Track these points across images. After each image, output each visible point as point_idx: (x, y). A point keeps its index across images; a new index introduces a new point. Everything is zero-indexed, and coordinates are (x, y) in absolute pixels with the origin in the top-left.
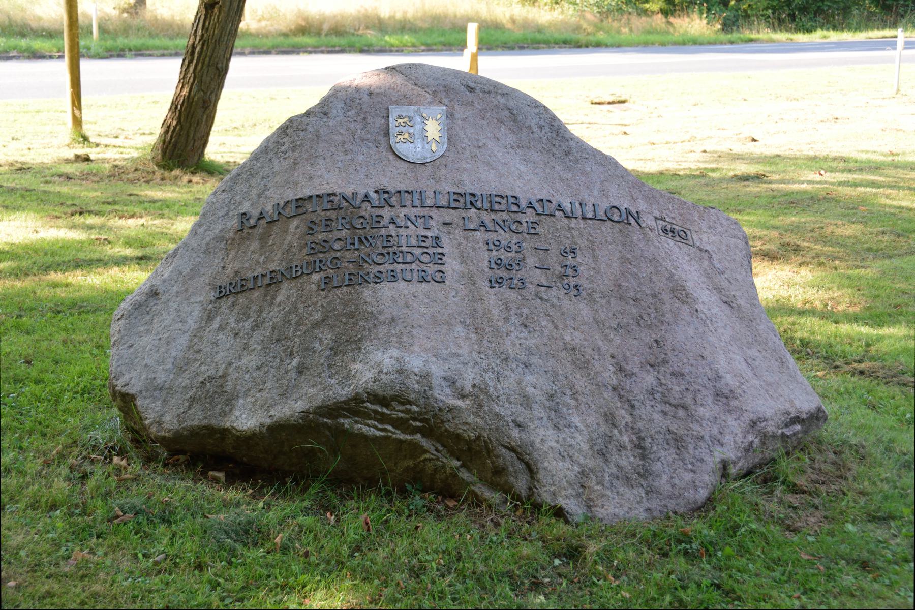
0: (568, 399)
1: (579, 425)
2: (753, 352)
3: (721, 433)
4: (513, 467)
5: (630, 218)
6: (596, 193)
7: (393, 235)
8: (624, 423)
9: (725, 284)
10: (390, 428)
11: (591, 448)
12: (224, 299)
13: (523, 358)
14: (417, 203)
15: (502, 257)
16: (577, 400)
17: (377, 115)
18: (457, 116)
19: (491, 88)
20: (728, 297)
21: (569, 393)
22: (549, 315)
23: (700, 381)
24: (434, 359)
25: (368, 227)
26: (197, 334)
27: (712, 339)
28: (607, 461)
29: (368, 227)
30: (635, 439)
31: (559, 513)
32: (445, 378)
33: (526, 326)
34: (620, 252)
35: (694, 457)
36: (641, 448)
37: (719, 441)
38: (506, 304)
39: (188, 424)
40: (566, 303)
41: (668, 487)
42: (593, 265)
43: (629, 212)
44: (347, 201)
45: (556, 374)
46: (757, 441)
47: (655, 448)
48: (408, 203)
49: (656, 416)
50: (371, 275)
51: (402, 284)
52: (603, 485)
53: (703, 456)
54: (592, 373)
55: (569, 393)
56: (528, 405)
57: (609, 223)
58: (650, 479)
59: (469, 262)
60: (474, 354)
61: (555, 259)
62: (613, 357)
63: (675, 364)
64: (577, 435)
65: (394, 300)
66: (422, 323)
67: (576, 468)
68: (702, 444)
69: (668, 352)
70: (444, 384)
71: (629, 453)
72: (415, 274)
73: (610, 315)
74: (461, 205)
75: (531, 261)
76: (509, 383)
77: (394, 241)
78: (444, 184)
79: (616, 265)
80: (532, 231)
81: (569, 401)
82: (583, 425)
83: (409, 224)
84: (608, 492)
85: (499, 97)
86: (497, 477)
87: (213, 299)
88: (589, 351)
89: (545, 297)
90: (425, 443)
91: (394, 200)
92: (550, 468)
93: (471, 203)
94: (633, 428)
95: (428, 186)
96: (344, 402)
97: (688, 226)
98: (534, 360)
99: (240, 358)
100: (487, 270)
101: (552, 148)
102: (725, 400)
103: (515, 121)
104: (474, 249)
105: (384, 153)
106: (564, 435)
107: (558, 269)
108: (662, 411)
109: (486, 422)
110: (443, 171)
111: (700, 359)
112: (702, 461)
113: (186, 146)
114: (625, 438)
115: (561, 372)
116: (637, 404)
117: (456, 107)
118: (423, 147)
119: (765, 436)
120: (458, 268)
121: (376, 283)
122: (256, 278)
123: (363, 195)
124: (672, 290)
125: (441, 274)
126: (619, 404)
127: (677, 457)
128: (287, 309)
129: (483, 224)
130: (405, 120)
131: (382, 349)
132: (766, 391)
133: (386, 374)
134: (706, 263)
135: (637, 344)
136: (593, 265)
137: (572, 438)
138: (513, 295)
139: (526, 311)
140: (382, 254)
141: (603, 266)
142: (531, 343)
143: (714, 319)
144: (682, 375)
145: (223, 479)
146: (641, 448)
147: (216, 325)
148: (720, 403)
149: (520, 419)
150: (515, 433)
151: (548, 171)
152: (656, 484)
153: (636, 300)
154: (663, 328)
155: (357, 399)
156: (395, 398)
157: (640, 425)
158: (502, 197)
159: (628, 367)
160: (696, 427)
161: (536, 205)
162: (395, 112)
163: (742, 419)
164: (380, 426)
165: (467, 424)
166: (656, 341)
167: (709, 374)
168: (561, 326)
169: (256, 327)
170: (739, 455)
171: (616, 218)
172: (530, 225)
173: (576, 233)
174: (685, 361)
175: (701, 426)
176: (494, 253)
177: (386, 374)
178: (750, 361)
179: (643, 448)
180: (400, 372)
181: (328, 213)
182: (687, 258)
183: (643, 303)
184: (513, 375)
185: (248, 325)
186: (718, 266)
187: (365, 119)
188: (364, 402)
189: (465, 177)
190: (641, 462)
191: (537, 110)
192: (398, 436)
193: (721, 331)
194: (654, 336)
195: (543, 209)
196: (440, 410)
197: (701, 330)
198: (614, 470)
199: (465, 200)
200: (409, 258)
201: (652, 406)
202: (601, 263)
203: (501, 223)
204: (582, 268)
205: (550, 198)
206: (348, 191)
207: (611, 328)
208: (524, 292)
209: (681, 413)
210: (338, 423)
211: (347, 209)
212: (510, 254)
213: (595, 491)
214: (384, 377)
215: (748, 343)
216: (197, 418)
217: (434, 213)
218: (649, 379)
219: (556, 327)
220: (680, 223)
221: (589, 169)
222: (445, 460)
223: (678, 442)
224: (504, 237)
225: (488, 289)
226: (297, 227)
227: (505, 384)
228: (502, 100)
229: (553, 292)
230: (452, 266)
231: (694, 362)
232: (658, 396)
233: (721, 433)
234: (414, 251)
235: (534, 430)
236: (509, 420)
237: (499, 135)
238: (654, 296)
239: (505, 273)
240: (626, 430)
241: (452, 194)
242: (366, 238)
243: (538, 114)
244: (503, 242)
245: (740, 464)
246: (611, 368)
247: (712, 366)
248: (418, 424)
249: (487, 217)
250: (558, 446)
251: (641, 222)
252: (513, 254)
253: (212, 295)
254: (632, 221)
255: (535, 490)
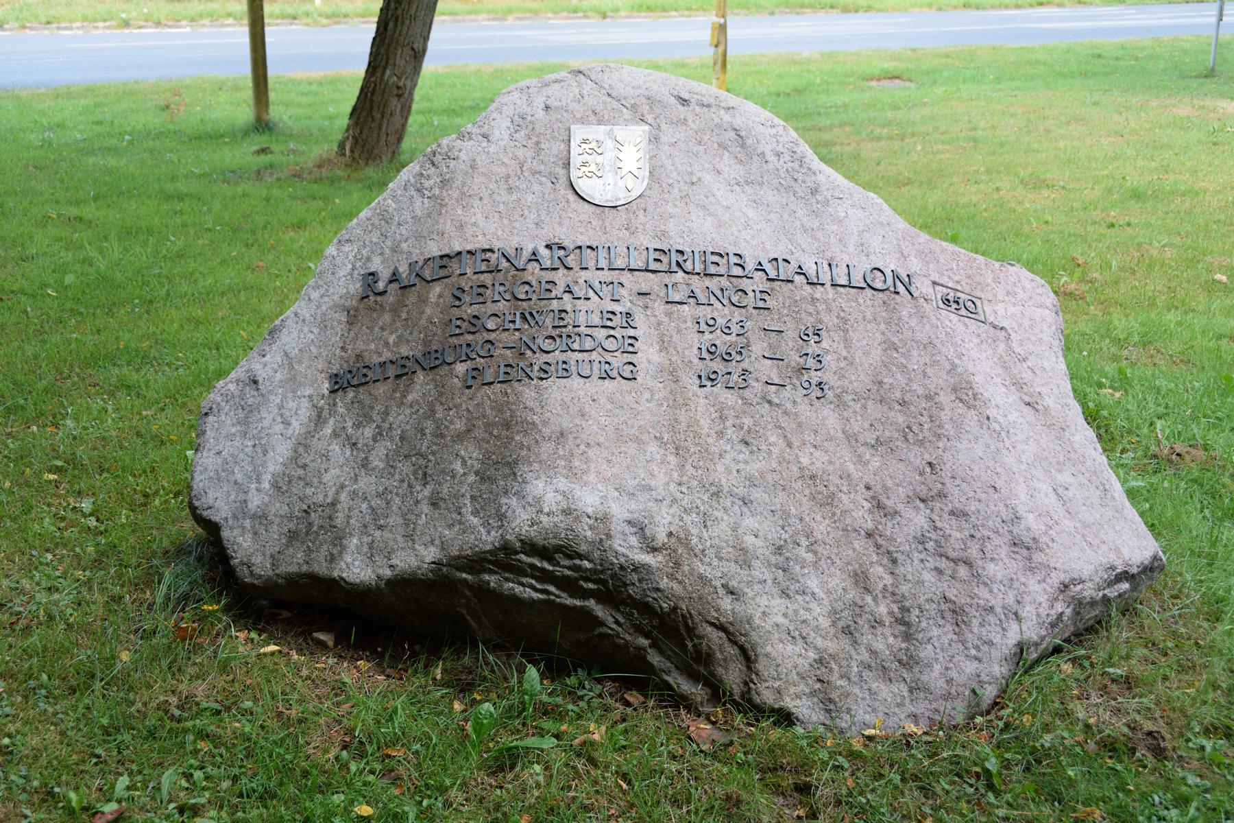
0: (802, 552)
1: (816, 590)
2: (1065, 478)
3: (1019, 602)
4: (721, 652)
5: (898, 284)
6: (851, 249)
7: (569, 309)
8: (881, 586)
9: (1028, 376)
10: (552, 589)
11: (834, 624)
12: (340, 393)
13: (740, 491)
14: (603, 263)
15: (717, 343)
16: (815, 553)
17: (554, 138)
18: (664, 139)
19: (712, 101)
20: (1032, 396)
21: (804, 542)
22: (781, 428)
23: (991, 523)
24: (617, 494)
25: (534, 297)
26: (303, 444)
27: (1009, 460)
28: (855, 643)
29: (534, 297)
30: (896, 610)
31: (785, 718)
32: (629, 522)
33: (746, 443)
34: (883, 334)
35: (980, 638)
36: (904, 624)
37: (1016, 614)
38: (721, 410)
39: (283, 569)
40: (803, 407)
41: (942, 683)
42: (844, 353)
43: (896, 277)
44: (508, 260)
45: (786, 515)
46: (1068, 611)
47: (924, 624)
48: (591, 264)
49: (928, 576)
50: (536, 368)
51: (576, 382)
52: (849, 679)
53: (992, 636)
54: (838, 512)
55: (804, 542)
56: (745, 561)
57: (869, 292)
58: (916, 670)
59: (671, 350)
60: (672, 485)
61: (791, 344)
62: (868, 488)
63: (956, 497)
64: (814, 605)
65: (565, 406)
66: (602, 440)
67: (812, 655)
68: (991, 618)
69: (947, 481)
70: (628, 529)
71: (888, 631)
72: (596, 366)
73: (866, 425)
74: (664, 267)
75: (759, 347)
76: (721, 530)
77: (569, 319)
78: (642, 237)
79: (877, 354)
80: (761, 304)
81: (804, 555)
82: (825, 586)
83: (591, 294)
84: (856, 690)
85: (722, 112)
86: (699, 664)
87: (326, 392)
88: (835, 479)
89: (776, 401)
90: (599, 611)
91: (571, 260)
92: (774, 654)
93: (678, 264)
94: (893, 594)
95: (617, 236)
96: (489, 552)
97: (978, 294)
98: (757, 494)
99: (356, 479)
100: (696, 361)
101: (793, 184)
102: (1025, 552)
103: (743, 146)
104: (679, 331)
105: (562, 192)
106: (796, 606)
107: (795, 359)
108: (936, 569)
109: (685, 588)
110: (642, 218)
111: (991, 491)
112: (990, 643)
113: (378, 141)
114: (882, 609)
115: (793, 511)
116: (900, 558)
117: (663, 127)
118: (615, 184)
119: (1080, 603)
120: (656, 358)
121: (542, 379)
122: (382, 365)
123: (530, 250)
124: (955, 390)
125: (631, 367)
126: (875, 558)
127: (955, 637)
128: (421, 411)
129: (693, 295)
130: (591, 146)
131: (544, 478)
132: (1083, 536)
133: (548, 515)
134: (1002, 346)
135: (903, 469)
136: (844, 353)
137: (807, 610)
138: (730, 398)
139: (748, 421)
140: (552, 337)
141: (859, 353)
142: (754, 467)
143: (1012, 431)
144: (966, 514)
145: (331, 644)
146: (904, 624)
147: (328, 430)
148: (1018, 557)
149: (733, 584)
150: (726, 603)
151: (786, 216)
152: (924, 678)
153: (903, 403)
154: (940, 444)
155: (506, 548)
156: (559, 549)
157: (904, 589)
158: (721, 255)
159: (889, 503)
160: (982, 592)
161: (767, 266)
162: (579, 133)
163: (1048, 580)
164: (538, 586)
165: (658, 590)
166: (930, 464)
167: (1004, 514)
168: (796, 444)
169: (378, 436)
170: (1043, 633)
171: (879, 285)
172: (759, 295)
173: (822, 307)
174: (971, 494)
175: (991, 591)
176: (707, 336)
177: (548, 515)
178: (1060, 490)
179: (907, 624)
180: (567, 512)
181: (482, 277)
182: (976, 340)
183: (913, 409)
184: (726, 518)
185: (368, 432)
186: (1018, 350)
187: (537, 143)
188: (517, 553)
189: (671, 227)
190: (904, 645)
191: (774, 131)
192: (563, 601)
193: (1020, 447)
194: (927, 456)
195: (778, 274)
196: (622, 568)
197: (993, 448)
198: (865, 656)
199: (670, 261)
200: (588, 344)
201: (922, 561)
202: (854, 352)
203: (718, 293)
204: (829, 358)
205: (788, 258)
206: (509, 245)
207: (866, 444)
208: (746, 393)
209: (963, 571)
210: (481, 580)
211: (508, 271)
212: (728, 338)
213: (837, 688)
214: (544, 519)
215: (1058, 463)
216: (295, 562)
217: (626, 278)
218: (918, 520)
219: (790, 445)
220: (967, 289)
221: (843, 214)
222: (628, 638)
223: (957, 615)
224: (722, 314)
225: (696, 388)
226: (440, 296)
227: (715, 531)
228: (727, 117)
229: (787, 392)
230: (648, 355)
231: (983, 496)
232: (930, 545)
233: (1019, 602)
234: (594, 334)
235: (753, 599)
236: (718, 583)
237: (721, 166)
238: (929, 397)
239: (722, 364)
240: (884, 597)
241: (651, 251)
242: (531, 314)
243: (775, 136)
244: (719, 321)
245: (1044, 646)
246: (866, 504)
247: (1008, 502)
248: (591, 586)
249: (698, 284)
250: (786, 622)
251: (912, 289)
252: (733, 338)
253: (326, 386)
254: (901, 288)
255: (752, 685)
